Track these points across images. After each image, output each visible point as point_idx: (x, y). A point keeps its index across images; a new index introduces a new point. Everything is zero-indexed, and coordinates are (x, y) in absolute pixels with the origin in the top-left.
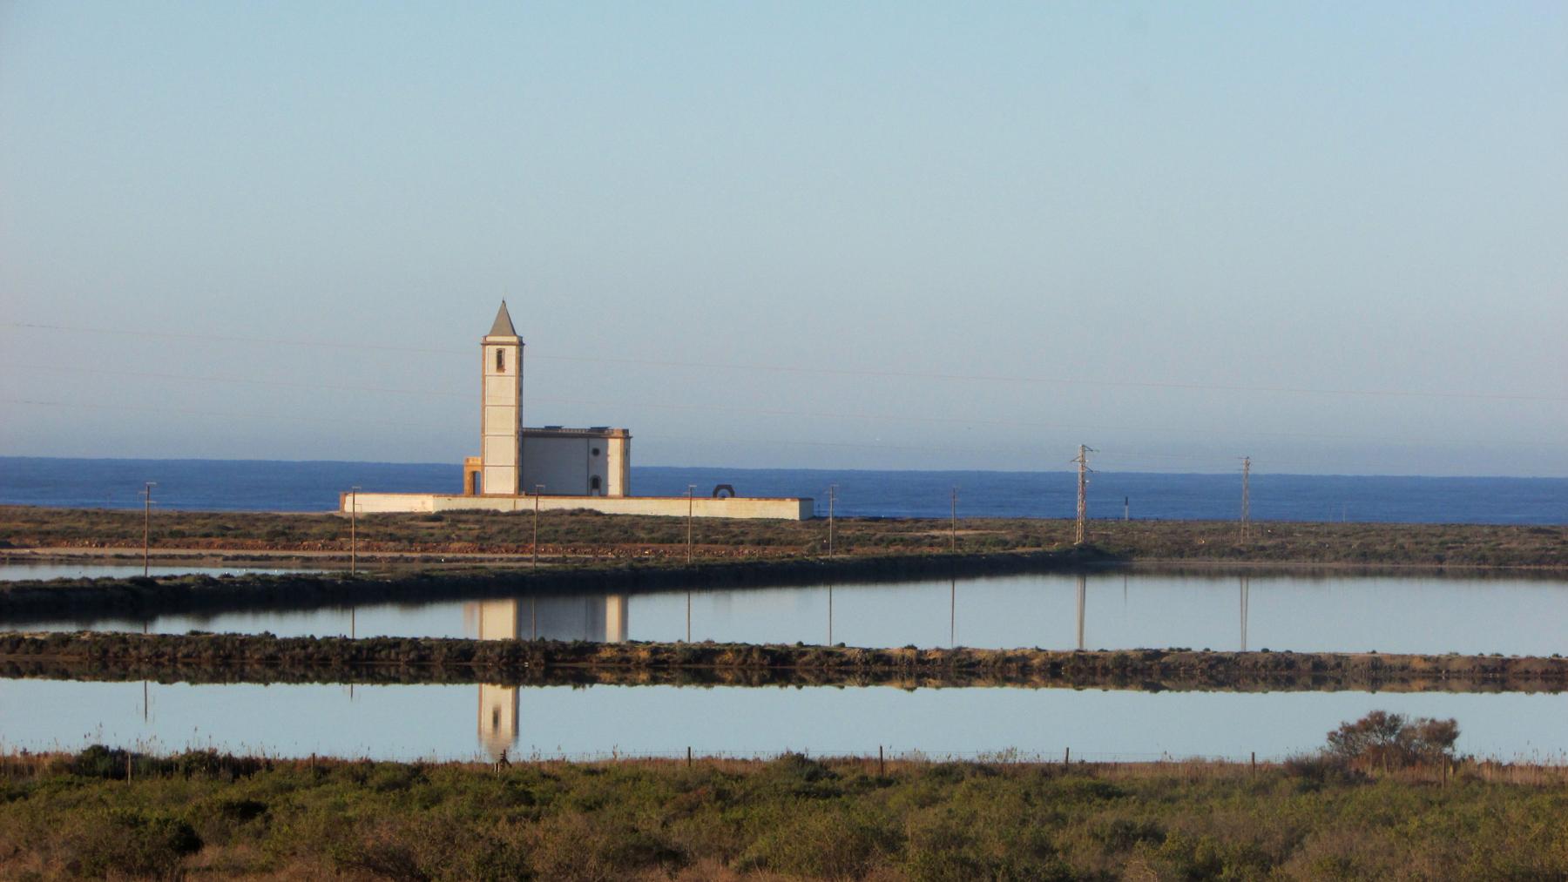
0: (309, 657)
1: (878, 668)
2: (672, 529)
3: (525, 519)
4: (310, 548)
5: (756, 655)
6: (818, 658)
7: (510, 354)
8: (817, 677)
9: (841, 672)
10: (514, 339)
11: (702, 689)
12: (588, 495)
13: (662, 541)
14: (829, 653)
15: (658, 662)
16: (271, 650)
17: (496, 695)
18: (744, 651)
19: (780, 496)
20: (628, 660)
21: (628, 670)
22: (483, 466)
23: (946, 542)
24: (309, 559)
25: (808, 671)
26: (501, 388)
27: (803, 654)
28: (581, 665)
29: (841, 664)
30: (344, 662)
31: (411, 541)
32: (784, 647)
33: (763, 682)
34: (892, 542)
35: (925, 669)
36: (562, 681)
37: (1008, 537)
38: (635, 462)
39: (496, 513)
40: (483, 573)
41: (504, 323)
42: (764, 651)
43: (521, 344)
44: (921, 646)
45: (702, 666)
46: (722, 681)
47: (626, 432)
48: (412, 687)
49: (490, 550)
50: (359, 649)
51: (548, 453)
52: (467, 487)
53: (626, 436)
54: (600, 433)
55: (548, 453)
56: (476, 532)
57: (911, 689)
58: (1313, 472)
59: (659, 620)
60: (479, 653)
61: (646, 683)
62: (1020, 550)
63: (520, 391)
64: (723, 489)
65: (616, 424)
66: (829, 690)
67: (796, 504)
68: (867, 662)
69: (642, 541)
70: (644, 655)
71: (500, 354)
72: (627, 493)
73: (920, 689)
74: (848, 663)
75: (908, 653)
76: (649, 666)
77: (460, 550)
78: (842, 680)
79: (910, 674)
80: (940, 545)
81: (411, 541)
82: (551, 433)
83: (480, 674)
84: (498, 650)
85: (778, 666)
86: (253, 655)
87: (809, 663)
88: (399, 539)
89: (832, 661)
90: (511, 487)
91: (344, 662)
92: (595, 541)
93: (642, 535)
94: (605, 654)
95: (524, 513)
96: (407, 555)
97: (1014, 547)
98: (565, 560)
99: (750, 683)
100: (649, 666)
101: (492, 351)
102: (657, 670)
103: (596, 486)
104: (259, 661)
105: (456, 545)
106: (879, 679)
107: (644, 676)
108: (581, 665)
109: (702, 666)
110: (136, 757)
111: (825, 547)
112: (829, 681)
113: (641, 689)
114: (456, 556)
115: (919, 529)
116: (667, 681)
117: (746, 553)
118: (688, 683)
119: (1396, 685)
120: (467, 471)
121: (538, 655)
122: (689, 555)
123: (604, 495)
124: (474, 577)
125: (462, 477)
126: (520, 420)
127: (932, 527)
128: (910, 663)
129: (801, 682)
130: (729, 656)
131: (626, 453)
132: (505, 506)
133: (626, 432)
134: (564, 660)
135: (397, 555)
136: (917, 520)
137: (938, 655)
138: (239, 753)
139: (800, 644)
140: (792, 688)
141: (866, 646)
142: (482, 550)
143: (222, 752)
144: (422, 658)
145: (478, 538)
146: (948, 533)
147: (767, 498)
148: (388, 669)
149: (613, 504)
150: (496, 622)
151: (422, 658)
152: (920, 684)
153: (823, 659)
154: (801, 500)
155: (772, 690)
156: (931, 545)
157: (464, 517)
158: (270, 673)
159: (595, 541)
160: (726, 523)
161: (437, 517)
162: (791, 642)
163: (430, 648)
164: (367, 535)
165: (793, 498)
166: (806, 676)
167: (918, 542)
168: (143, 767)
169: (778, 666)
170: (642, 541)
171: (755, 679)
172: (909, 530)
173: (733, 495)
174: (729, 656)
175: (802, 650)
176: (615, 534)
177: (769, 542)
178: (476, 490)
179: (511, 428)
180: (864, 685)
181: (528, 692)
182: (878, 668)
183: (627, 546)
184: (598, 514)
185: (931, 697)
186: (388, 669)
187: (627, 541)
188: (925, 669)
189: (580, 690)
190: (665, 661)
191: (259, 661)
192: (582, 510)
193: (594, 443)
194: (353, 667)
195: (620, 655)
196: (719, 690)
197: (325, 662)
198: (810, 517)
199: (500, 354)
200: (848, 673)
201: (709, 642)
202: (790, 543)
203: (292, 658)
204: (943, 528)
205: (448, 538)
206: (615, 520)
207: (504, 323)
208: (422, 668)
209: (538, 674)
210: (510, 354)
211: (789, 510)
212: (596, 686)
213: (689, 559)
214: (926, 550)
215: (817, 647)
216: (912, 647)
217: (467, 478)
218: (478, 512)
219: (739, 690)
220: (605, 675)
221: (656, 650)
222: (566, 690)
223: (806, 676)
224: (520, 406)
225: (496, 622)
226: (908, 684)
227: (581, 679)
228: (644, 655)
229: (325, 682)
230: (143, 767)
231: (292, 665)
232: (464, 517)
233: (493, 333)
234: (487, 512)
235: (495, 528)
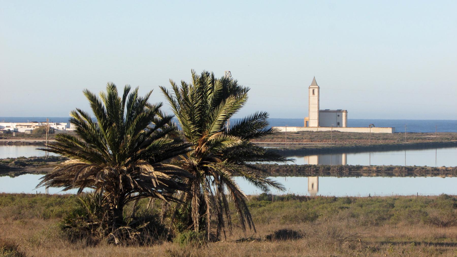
0: (287, 170)
1: (435, 172)
2: (360, 136)
3: (320, 133)
4: (267, 141)
5: (404, 169)
6: (420, 169)
7: (316, 90)
8: (420, 175)
9: (426, 173)
10: (317, 87)
11: (389, 178)
12: (337, 127)
13: (359, 139)
14: (423, 168)
15: (378, 171)
16: (278, 168)
17: (313, 179)
18: (401, 168)
19: (387, 127)
20: (371, 170)
21: (371, 173)
22: (309, 119)
23: (433, 139)
24: (269, 144)
25: (418, 173)
26: (314, 100)
27: (416, 168)
28: (358, 171)
29: (426, 171)
30: (297, 171)
31: (293, 139)
32: (411, 167)
33: (405, 176)
34: (418, 139)
35: (448, 172)
36: (353, 176)
37: (449, 137)
38: (348, 118)
39: (313, 132)
40: (313, 148)
41: (314, 82)
42: (406, 168)
43: (319, 88)
44: (447, 166)
45: (389, 172)
46: (395, 176)
47: (346, 111)
48: (434, 178)
49: (314, 141)
50: (300, 168)
51: (325, 116)
52: (305, 125)
53: (346, 112)
54: (340, 111)
55: (325, 116)
56: (309, 137)
57: (444, 178)
58: (400, 119)
59: (353, 160)
60: (332, 169)
61: (375, 176)
62: (452, 141)
63: (319, 100)
64: (372, 125)
65: (343, 109)
66: (423, 178)
67: (391, 129)
68: (433, 171)
69: (353, 139)
70: (375, 169)
71: (313, 90)
72: (347, 127)
73: (446, 178)
74: (428, 171)
75: (443, 168)
76: (376, 172)
77: (306, 142)
78: (426, 175)
79: (444, 174)
80: (431, 139)
81: (293, 139)
82: (327, 111)
83: (332, 174)
84: (337, 168)
85: (410, 172)
86: (273, 169)
87: (418, 171)
88: (290, 139)
89: (424, 170)
90: (316, 125)
91: (297, 171)
92: (341, 139)
93: (353, 137)
94: (365, 169)
95: (320, 132)
96: (282, 143)
97: (451, 140)
98: (335, 144)
99: (402, 176)
100: (376, 172)
101: (311, 90)
102: (378, 173)
103: (339, 124)
104: (275, 171)
105: (305, 140)
106: (436, 175)
107: (375, 174)
108: (358, 171)
109: (389, 172)
110: (274, 196)
111: (402, 140)
112: (423, 176)
113: (373, 178)
114: (306, 143)
115: (424, 135)
116: (381, 176)
117: (381, 142)
118: (386, 176)
119: (36, 174)
120: (305, 121)
121: (347, 169)
122: (354, 143)
123: (342, 127)
124: (317, 149)
125: (304, 123)
126: (319, 108)
127: (427, 135)
128: (444, 171)
129: (415, 176)
130: (397, 169)
131: (346, 116)
132: (315, 130)
133: (346, 111)
134: (354, 170)
135: (291, 143)
136: (423, 133)
137: (451, 169)
138: (301, 194)
139: (415, 166)
140: (413, 177)
141: (432, 166)
142: (312, 141)
143: (296, 195)
144: (317, 170)
145: (310, 138)
146: (432, 136)
147: (383, 127)
148: (308, 173)
149: (343, 129)
150: (313, 160)
151: (317, 170)
152: (446, 176)
153: (421, 170)
154: (392, 128)
155: (408, 178)
156: (429, 140)
157: (304, 133)
158: (277, 174)
159: (341, 139)
160: (373, 134)
161: (298, 133)
162: (412, 165)
163: (319, 167)
164: (281, 138)
165: (390, 127)
166: (417, 174)
167: (425, 139)
168: (276, 199)
169: (410, 172)
170: (353, 139)
171: (404, 175)
172: (421, 135)
173: (374, 127)
174: (397, 169)
175: (415, 167)
176: (346, 137)
177: (386, 139)
178: (307, 126)
179: (316, 110)
180: (432, 176)
181: (320, 178)
182: (435, 172)
183: (349, 140)
184: (339, 132)
185: (429, 179)
186: (308, 173)
187: (349, 139)
188: (448, 172)
189: (358, 178)
190: (380, 171)
191: (275, 171)
192: (335, 131)
193: (338, 114)
194: (299, 172)
195: (368, 169)
196: (394, 178)
197: (292, 171)
198: (394, 132)
199: (313, 90)
200: (428, 173)
201: (391, 165)
202: (392, 139)
203: (283, 170)
204: (430, 135)
205: (303, 138)
206: (344, 134)
207: (314, 82)
208: (317, 173)
209: (347, 174)
210: (316, 90)
211: (389, 131)
212: (362, 177)
213: (370, 144)
214: (428, 141)
215: (419, 167)
216: (444, 167)
217: (305, 123)
218: (308, 131)
219: (399, 178)
220: (364, 174)
221: (378, 168)
222: (354, 178)
223: (417, 174)
224: (319, 104)
225: (313, 160)
226: (443, 176)
227: (358, 175)
228: (375, 169)
229: (292, 176)
230: (276, 199)
231: (283, 172)
232: (304, 133)
233: (312, 85)
234: (310, 132)
235: (314, 136)
